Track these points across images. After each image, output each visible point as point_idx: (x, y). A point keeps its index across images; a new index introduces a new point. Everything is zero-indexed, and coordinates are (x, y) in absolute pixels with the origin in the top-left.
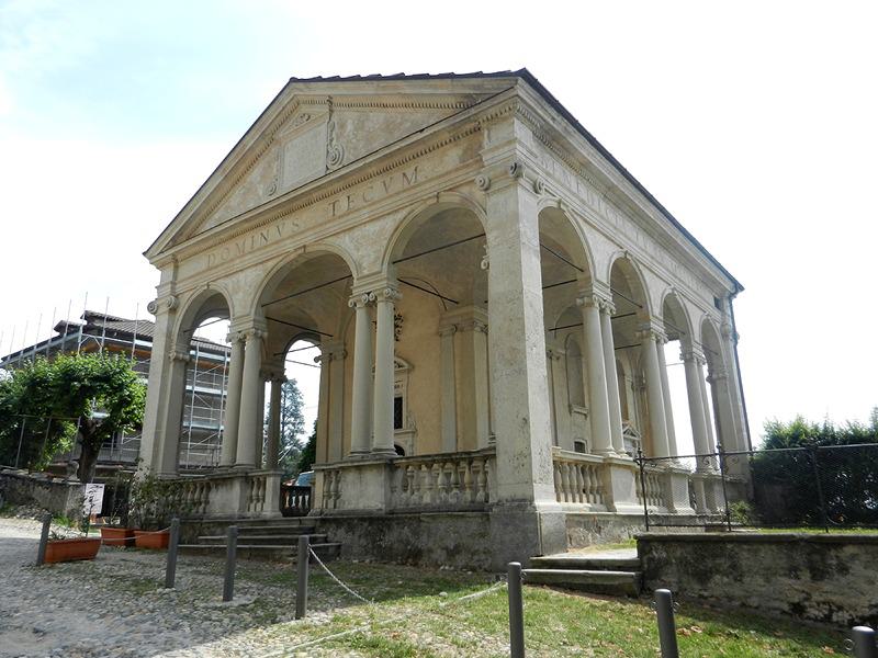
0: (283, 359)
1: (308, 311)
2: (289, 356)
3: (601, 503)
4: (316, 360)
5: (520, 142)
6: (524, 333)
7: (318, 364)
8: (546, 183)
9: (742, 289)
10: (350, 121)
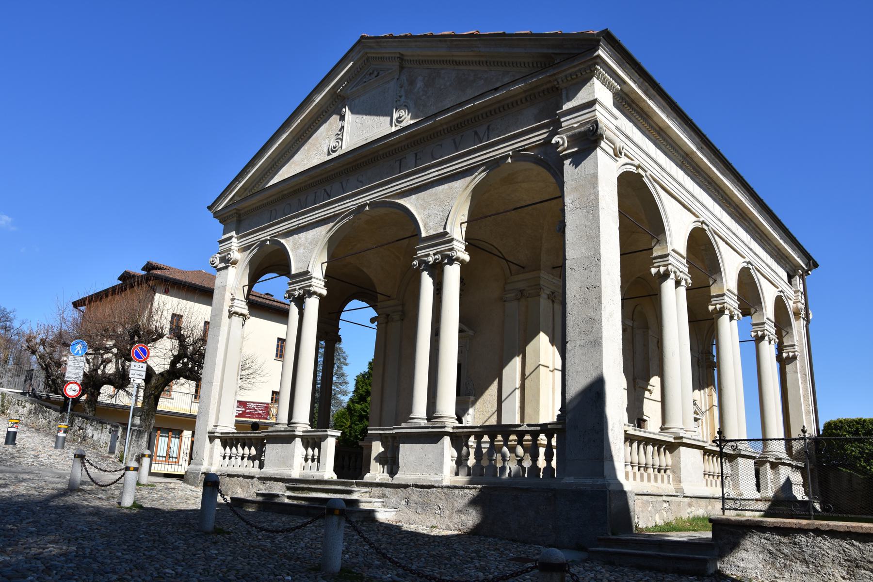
0: (338, 319)
1: (365, 270)
2: (343, 316)
3: (669, 482)
4: (372, 320)
5: (600, 104)
6: (600, 302)
7: (374, 325)
8: (626, 147)
9: (816, 265)
10: (420, 78)
